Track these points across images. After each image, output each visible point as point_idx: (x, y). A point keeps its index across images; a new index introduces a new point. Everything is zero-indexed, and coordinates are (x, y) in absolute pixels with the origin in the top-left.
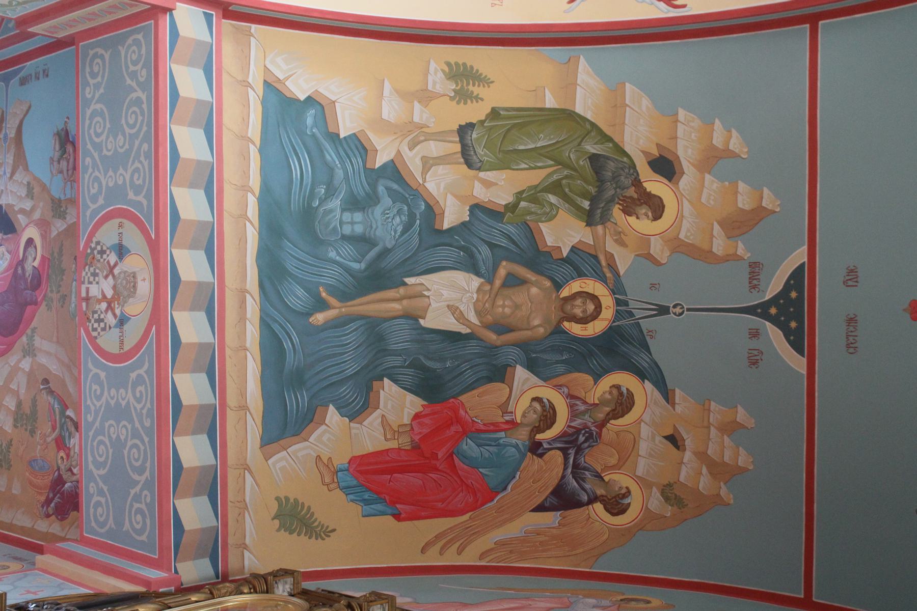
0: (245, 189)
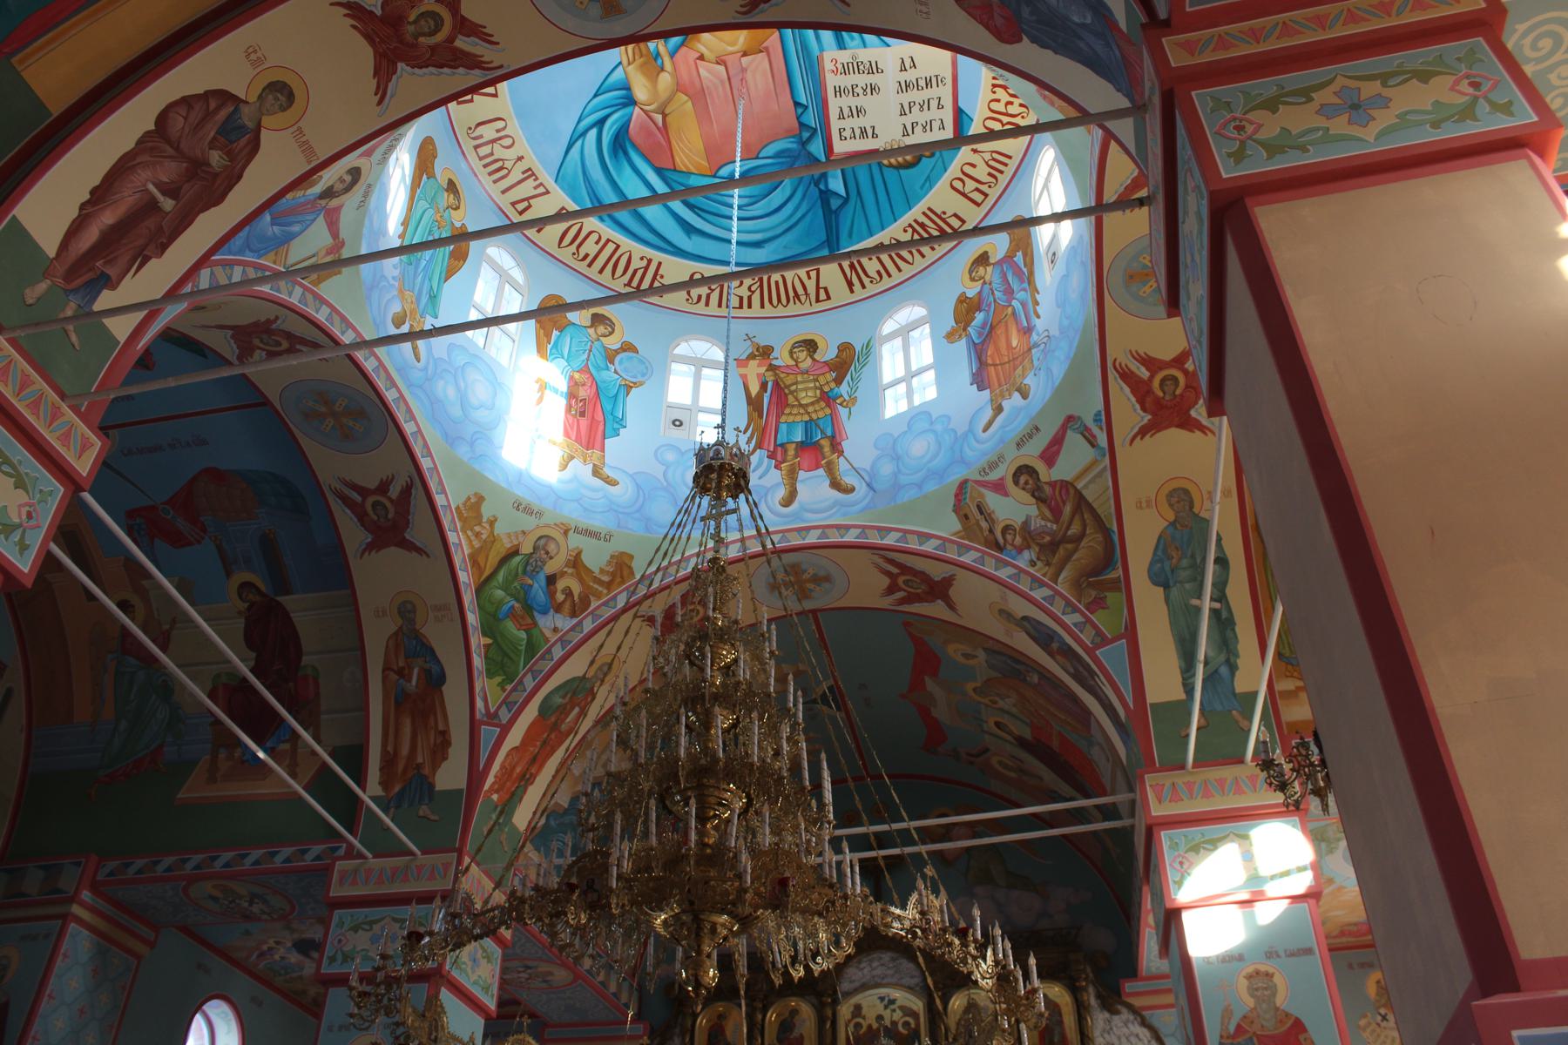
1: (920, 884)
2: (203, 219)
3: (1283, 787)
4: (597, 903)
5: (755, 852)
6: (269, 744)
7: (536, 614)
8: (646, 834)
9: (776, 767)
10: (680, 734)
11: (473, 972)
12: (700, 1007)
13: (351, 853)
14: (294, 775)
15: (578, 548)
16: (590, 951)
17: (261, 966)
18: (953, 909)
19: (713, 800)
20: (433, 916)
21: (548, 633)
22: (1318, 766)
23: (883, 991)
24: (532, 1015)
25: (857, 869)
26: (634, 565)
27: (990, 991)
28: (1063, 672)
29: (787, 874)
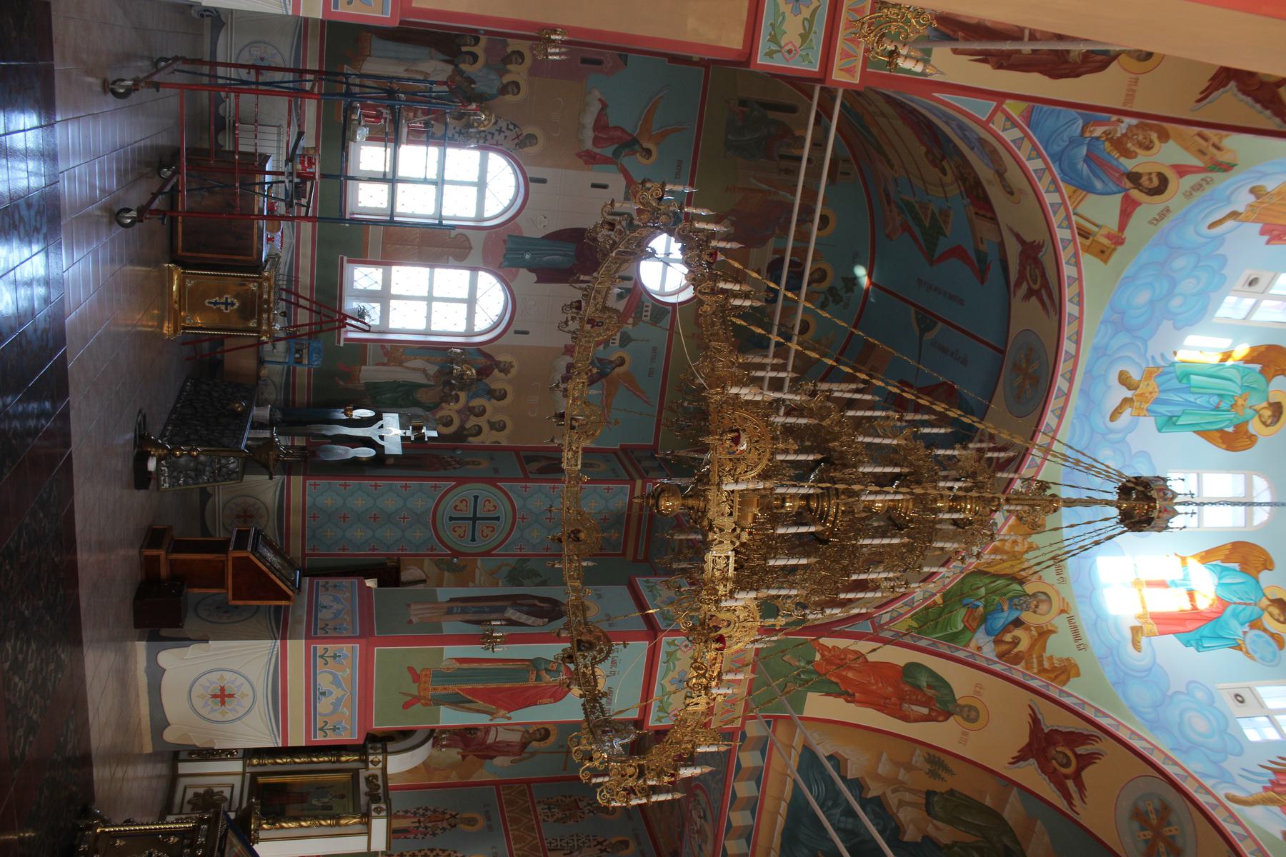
0: (780, 799)
2: (1036, 77)
7: (983, 627)
15: (1056, 627)
21: (973, 644)
26: (1073, 680)
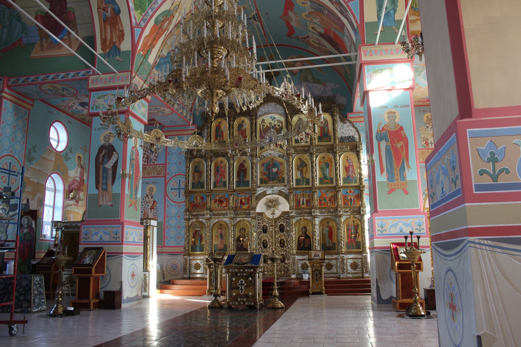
1: (285, 79)
3: (408, 51)
4: (179, 87)
5: (230, 69)
6: (60, 37)
8: (194, 64)
9: (237, 41)
10: (204, 29)
11: (139, 110)
12: (213, 119)
13: (94, 73)
14: (71, 47)
16: (177, 102)
17: (70, 111)
18: (295, 88)
19: (216, 52)
20: (125, 92)
22: (421, 45)
23: (272, 115)
24: (160, 124)
25: (264, 75)
27: (306, 114)
28: (336, 10)
29: (241, 76)
